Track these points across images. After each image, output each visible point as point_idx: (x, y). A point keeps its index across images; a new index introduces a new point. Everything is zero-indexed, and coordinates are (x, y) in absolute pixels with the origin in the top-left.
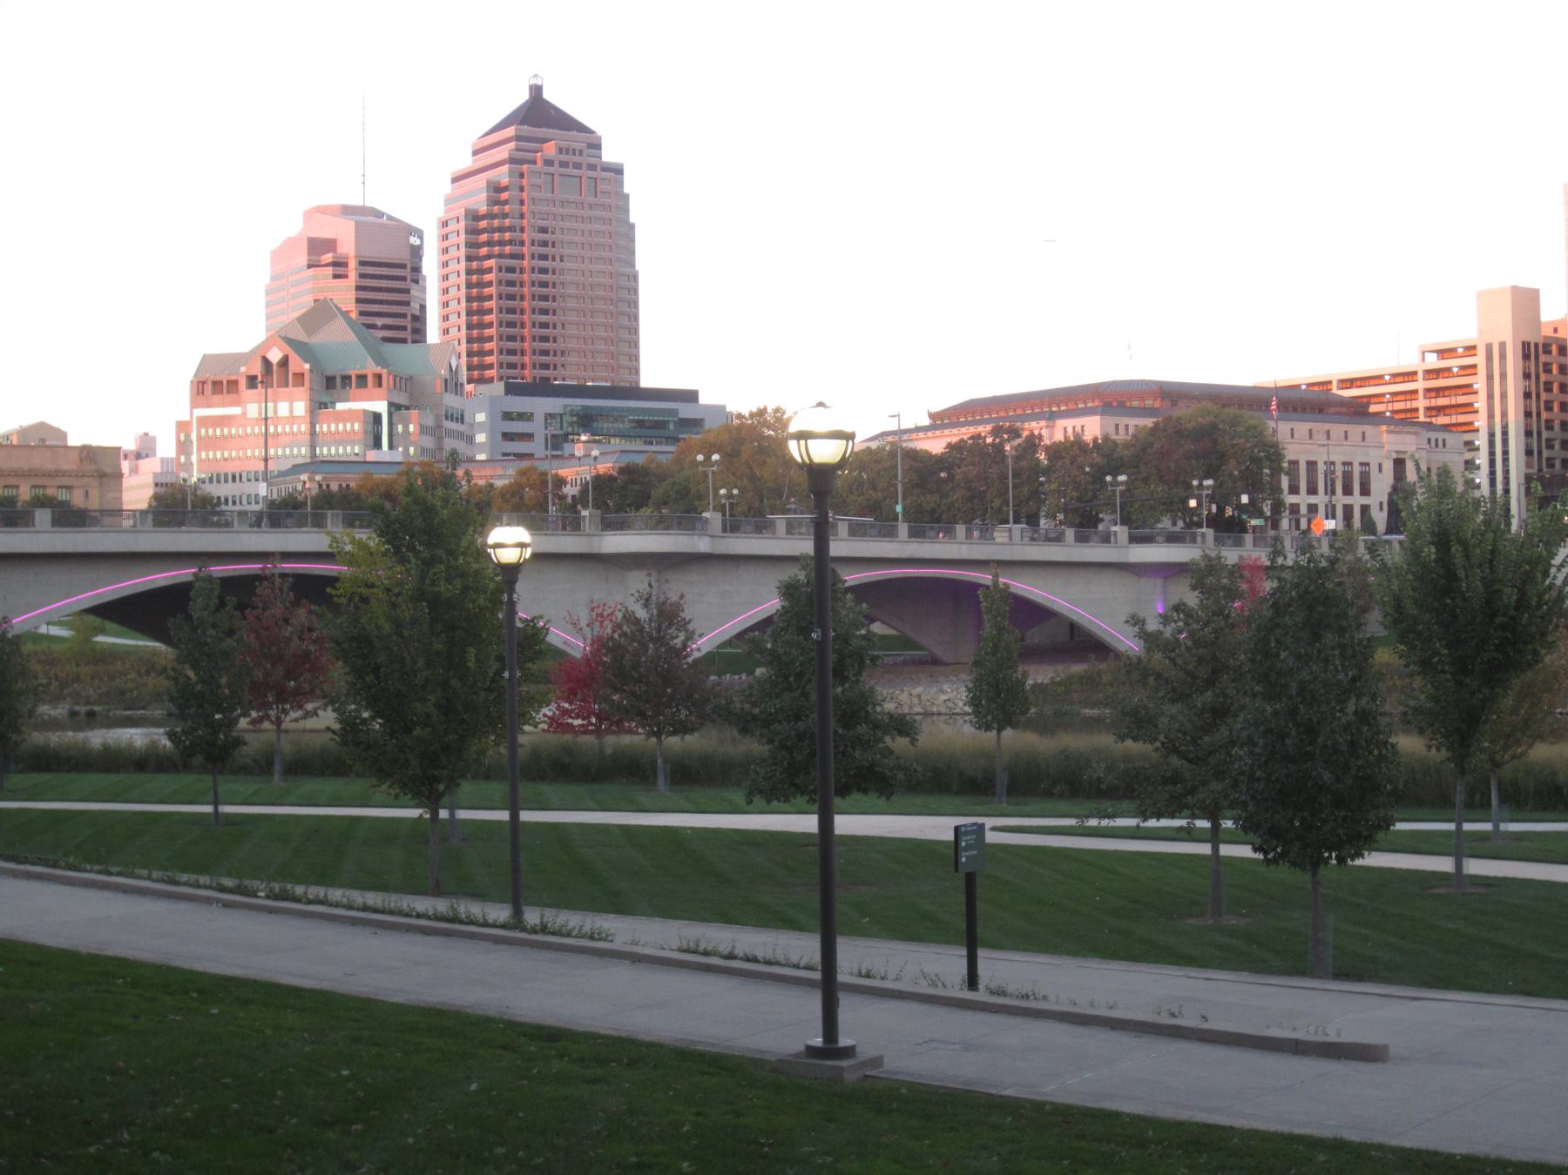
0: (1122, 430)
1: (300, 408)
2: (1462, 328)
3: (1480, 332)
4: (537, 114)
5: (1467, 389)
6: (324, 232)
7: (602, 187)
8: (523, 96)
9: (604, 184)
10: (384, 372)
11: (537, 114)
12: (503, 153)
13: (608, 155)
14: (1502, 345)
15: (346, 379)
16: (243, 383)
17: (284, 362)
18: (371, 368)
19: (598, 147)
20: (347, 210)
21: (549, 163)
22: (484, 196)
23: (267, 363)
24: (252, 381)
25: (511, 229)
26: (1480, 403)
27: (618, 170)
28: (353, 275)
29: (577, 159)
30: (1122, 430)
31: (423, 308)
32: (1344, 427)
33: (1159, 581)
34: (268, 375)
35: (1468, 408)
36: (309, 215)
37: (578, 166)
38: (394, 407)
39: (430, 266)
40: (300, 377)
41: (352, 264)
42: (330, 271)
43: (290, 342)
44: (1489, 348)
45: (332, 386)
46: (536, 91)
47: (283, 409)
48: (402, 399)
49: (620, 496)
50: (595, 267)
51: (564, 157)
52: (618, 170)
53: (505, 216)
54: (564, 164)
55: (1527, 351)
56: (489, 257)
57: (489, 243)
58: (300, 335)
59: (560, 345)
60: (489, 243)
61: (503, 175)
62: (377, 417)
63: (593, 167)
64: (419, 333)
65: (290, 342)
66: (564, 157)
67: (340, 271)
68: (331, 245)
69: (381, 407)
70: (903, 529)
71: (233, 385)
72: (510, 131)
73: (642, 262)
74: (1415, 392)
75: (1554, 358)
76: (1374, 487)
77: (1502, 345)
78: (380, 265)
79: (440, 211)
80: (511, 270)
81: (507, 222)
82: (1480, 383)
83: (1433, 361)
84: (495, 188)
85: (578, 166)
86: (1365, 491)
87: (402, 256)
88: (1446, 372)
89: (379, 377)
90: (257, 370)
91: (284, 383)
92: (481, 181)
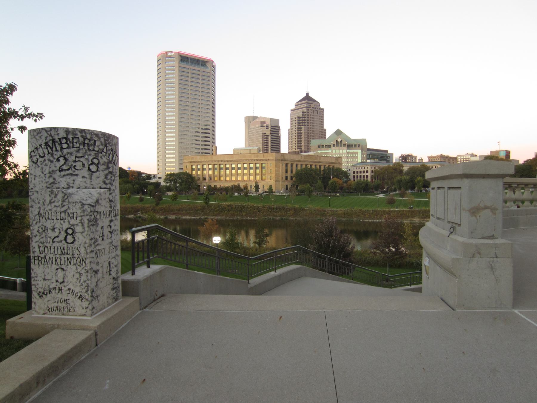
4: (307, 98)
8: (305, 95)
9: (321, 112)
11: (307, 98)
13: (321, 106)
22: (301, 113)
24: (334, 145)
27: (323, 110)
28: (270, 129)
41: (270, 126)
42: (265, 127)
46: (307, 94)
47: (341, 151)
49: (38, 134)
52: (323, 110)
61: (305, 110)
71: (330, 146)
72: (305, 101)
84: (303, 112)
90: (335, 143)
91: (341, 146)
92: (301, 111)
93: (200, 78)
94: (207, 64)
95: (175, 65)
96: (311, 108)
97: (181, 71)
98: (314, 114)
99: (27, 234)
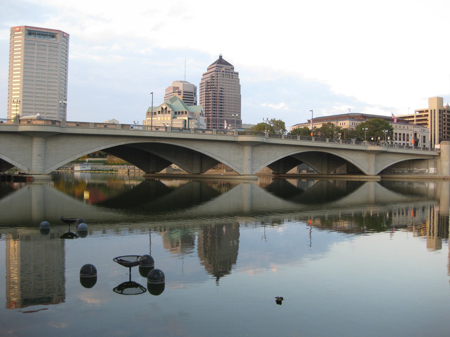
0: (354, 124)
1: (169, 118)
2: (425, 106)
3: (429, 107)
4: (221, 61)
5: (426, 120)
6: (176, 86)
7: (234, 77)
8: (218, 58)
10: (187, 111)
11: (221, 61)
12: (214, 69)
13: (235, 70)
14: (435, 110)
15: (179, 113)
16: (157, 113)
17: (166, 108)
18: (184, 110)
19: (233, 69)
20: (181, 82)
21: (223, 72)
23: (162, 108)
24: (159, 112)
25: (215, 88)
26: (429, 123)
27: (237, 74)
28: (182, 94)
29: (229, 71)
30: (354, 124)
31: (196, 102)
32: (404, 125)
33: (374, 155)
34: (163, 111)
35: (426, 124)
36: (173, 82)
37: (229, 72)
38: (189, 119)
39: (198, 93)
40: (169, 111)
41: (182, 92)
43: (167, 104)
44: (431, 111)
45: (177, 113)
46: (221, 57)
48: (191, 117)
50: (232, 85)
51: (226, 71)
52: (237, 74)
53: (214, 85)
54: (226, 72)
55: (440, 111)
56: (210, 91)
57: (210, 88)
58: (170, 103)
59: (224, 110)
60: (210, 88)
62: (185, 121)
63: (232, 73)
64: (195, 104)
65: (167, 104)
66: (226, 71)
67: (180, 93)
68: (178, 88)
69: (186, 118)
70: (313, 139)
72: (215, 65)
73: (242, 93)
74: (414, 121)
75: (446, 113)
76: (410, 139)
77: (435, 110)
78: (188, 92)
79: (200, 81)
80: (214, 94)
81: (214, 87)
82: (429, 118)
83: (418, 114)
85: (229, 72)
86: (408, 140)
87: (192, 90)
88: (421, 116)
89: (186, 112)
90: (160, 110)
91: (166, 113)
92: (209, 75)
93: (36, 51)
94: (58, 36)
95: (20, 38)
96: (221, 72)
97: (27, 44)
98: (225, 79)
99: (378, 216)
